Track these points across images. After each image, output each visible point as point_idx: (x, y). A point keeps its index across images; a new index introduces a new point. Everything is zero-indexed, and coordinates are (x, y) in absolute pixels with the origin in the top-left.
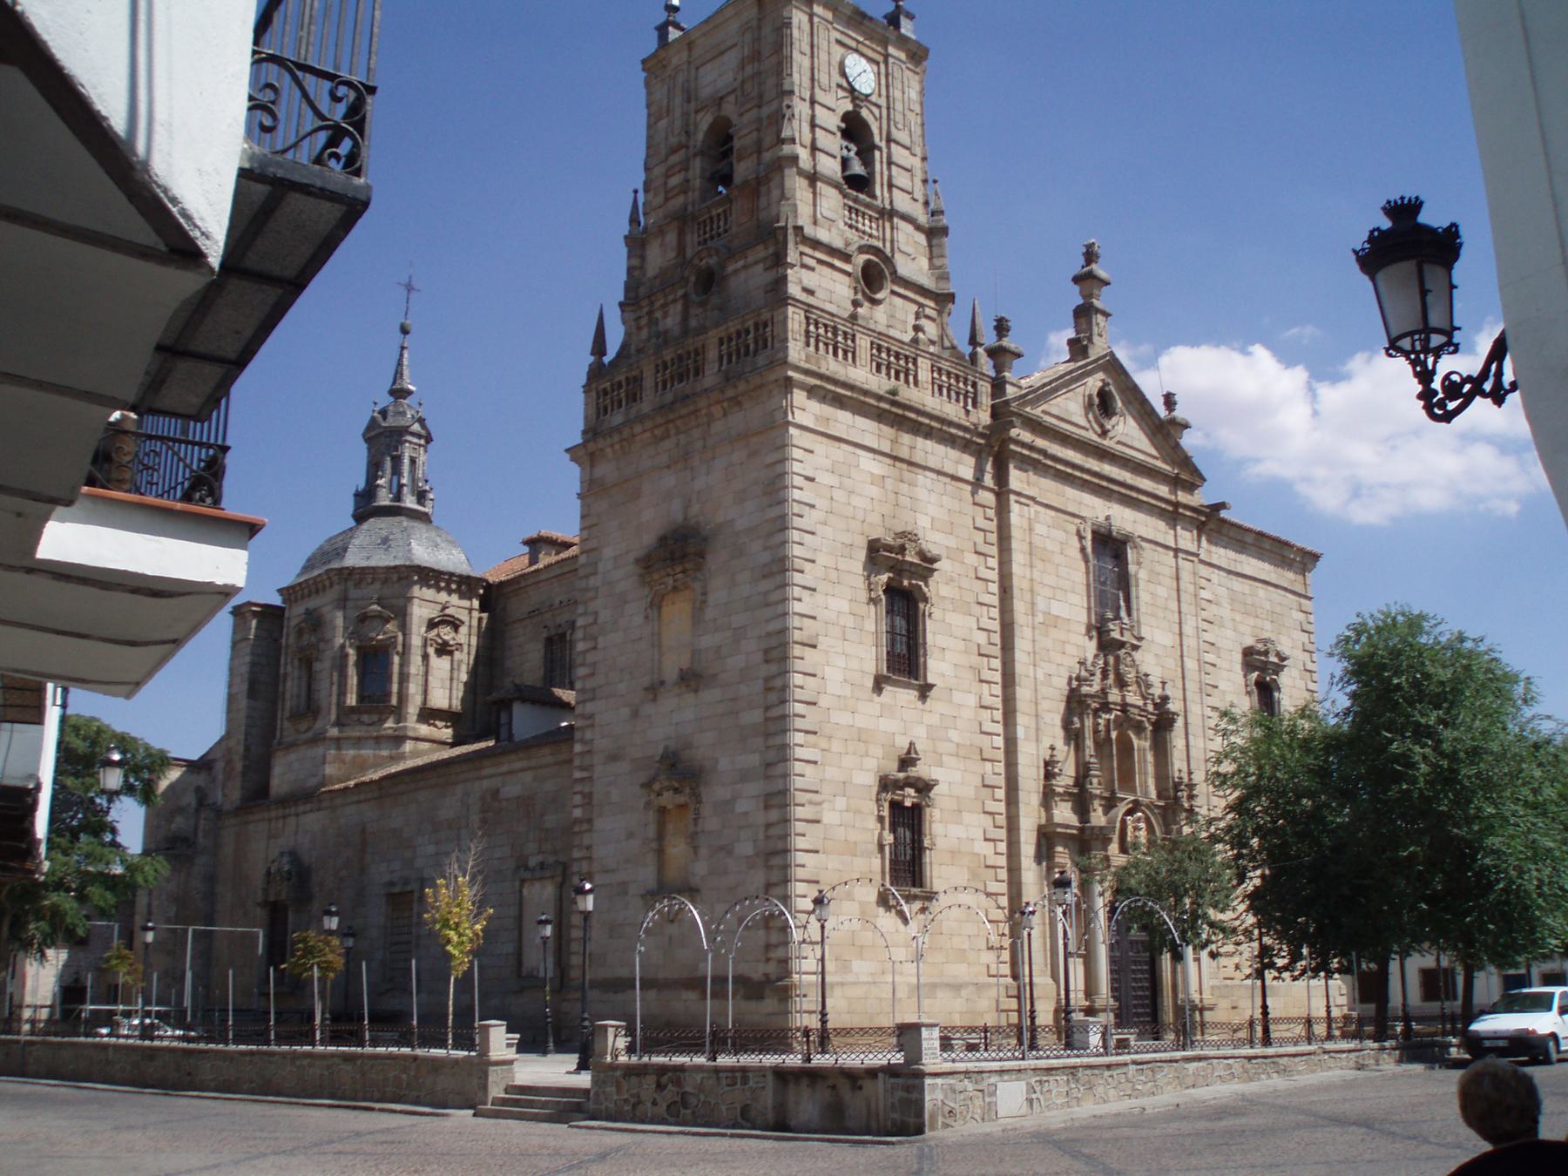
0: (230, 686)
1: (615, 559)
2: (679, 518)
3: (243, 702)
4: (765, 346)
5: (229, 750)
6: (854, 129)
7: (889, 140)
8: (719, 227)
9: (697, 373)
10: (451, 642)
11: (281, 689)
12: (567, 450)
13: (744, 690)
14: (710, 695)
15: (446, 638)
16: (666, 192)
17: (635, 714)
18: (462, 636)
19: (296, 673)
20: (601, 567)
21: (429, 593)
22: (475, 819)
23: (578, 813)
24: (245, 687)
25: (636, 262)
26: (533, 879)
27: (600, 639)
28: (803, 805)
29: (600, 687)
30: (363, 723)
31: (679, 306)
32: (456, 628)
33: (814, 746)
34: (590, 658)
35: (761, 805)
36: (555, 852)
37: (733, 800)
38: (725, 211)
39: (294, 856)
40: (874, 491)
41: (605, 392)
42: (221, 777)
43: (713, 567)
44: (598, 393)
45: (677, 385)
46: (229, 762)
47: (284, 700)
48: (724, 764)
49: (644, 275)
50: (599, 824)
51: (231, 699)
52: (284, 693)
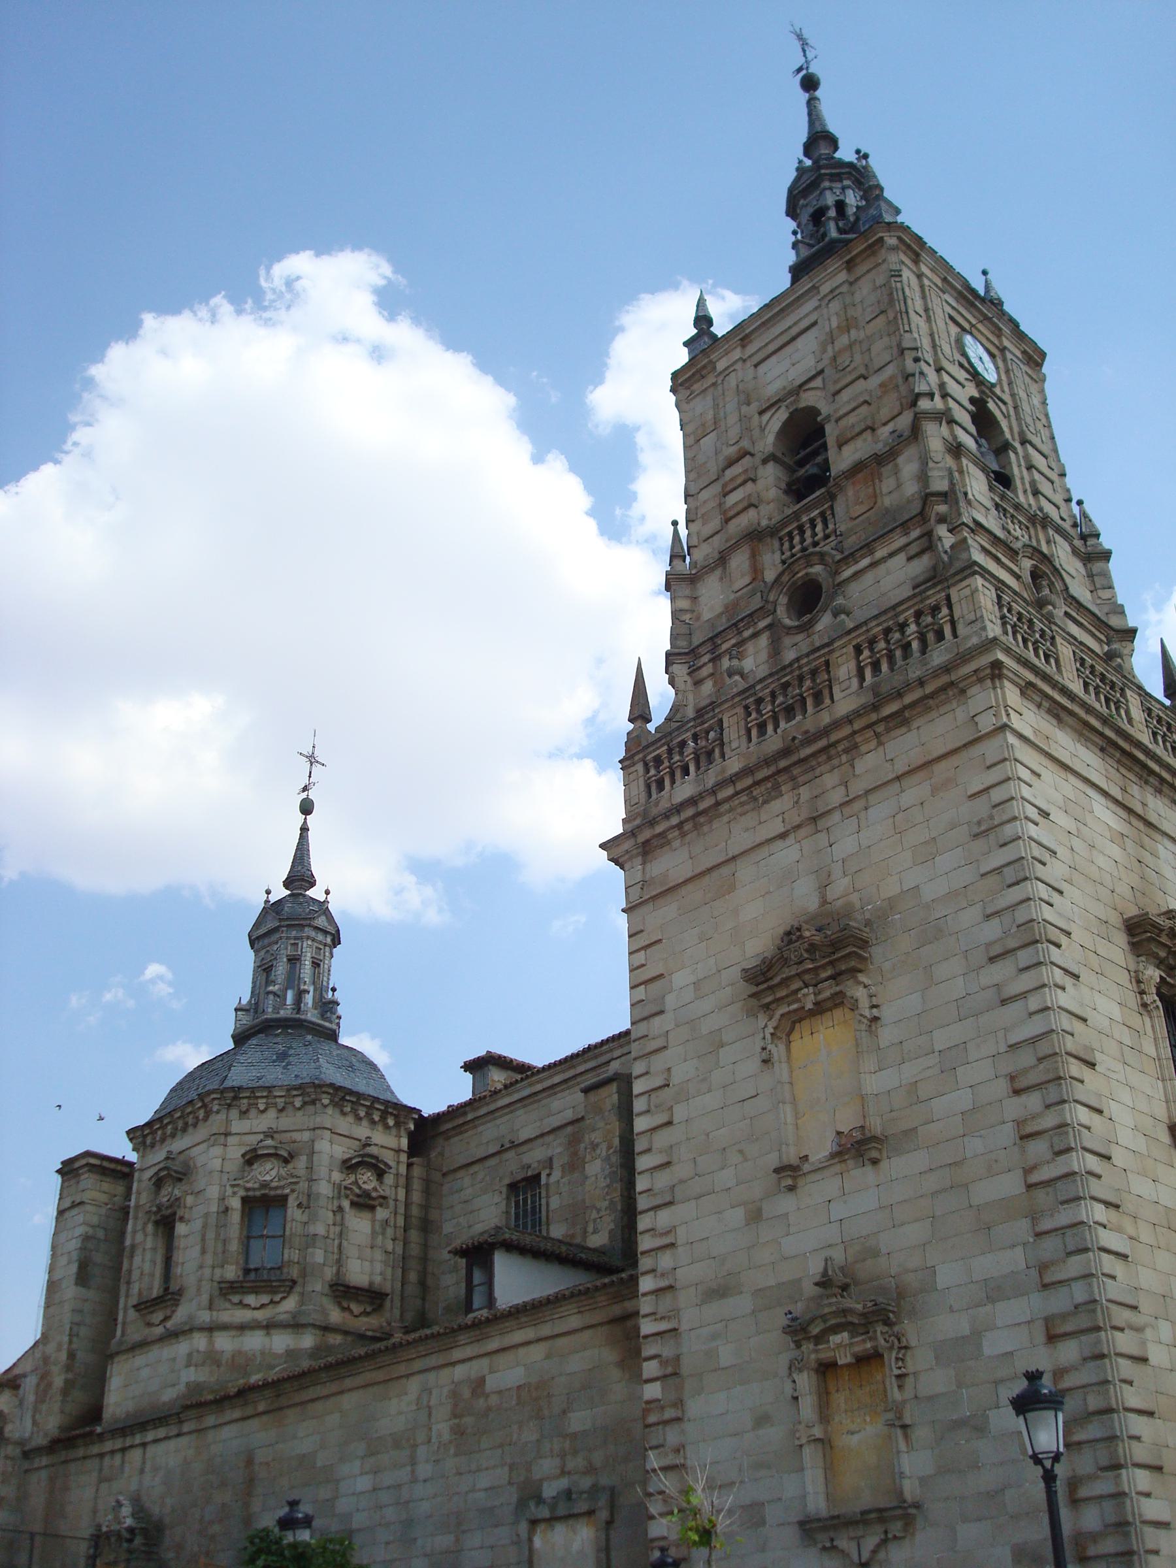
0: (51, 1270)
1: (697, 984)
2: (813, 904)
3: (70, 1291)
4: (940, 636)
5: (46, 1360)
6: (983, 421)
7: (1024, 442)
8: (814, 534)
9: (818, 697)
10: (374, 1194)
11: (125, 1266)
12: (603, 846)
13: (975, 1145)
14: (896, 1166)
15: (365, 1186)
16: (724, 512)
17: (755, 1216)
18: (388, 1185)
19: (149, 1244)
20: (671, 1001)
21: (344, 1124)
22: (442, 1428)
23: (653, 1391)
24: (74, 1268)
25: (684, 604)
26: (552, 1520)
27: (676, 1109)
28: (1122, 1330)
29: (682, 1182)
30: (248, 1306)
31: (764, 641)
32: (380, 1175)
33: (1119, 1230)
34: (662, 1139)
35: (1041, 1337)
36: (591, 1470)
37: (977, 1334)
38: (823, 515)
39: (139, 1510)
40: (1115, 851)
41: (658, 761)
42: (31, 1398)
43: (887, 966)
44: (646, 765)
45: (783, 725)
46: (44, 1377)
47: (128, 1283)
48: (946, 1276)
49: (698, 618)
50: (695, 1407)
51: (52, 1287)
52: (130, 1271)
